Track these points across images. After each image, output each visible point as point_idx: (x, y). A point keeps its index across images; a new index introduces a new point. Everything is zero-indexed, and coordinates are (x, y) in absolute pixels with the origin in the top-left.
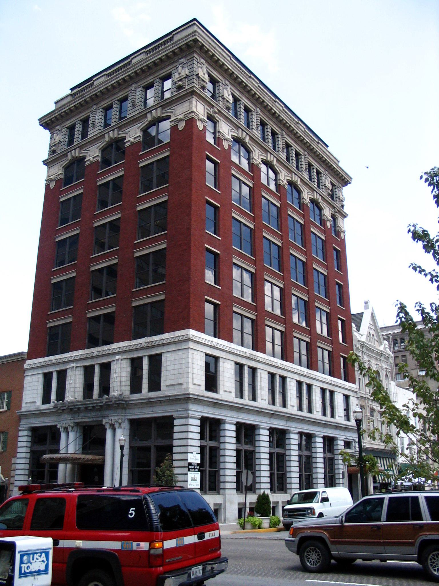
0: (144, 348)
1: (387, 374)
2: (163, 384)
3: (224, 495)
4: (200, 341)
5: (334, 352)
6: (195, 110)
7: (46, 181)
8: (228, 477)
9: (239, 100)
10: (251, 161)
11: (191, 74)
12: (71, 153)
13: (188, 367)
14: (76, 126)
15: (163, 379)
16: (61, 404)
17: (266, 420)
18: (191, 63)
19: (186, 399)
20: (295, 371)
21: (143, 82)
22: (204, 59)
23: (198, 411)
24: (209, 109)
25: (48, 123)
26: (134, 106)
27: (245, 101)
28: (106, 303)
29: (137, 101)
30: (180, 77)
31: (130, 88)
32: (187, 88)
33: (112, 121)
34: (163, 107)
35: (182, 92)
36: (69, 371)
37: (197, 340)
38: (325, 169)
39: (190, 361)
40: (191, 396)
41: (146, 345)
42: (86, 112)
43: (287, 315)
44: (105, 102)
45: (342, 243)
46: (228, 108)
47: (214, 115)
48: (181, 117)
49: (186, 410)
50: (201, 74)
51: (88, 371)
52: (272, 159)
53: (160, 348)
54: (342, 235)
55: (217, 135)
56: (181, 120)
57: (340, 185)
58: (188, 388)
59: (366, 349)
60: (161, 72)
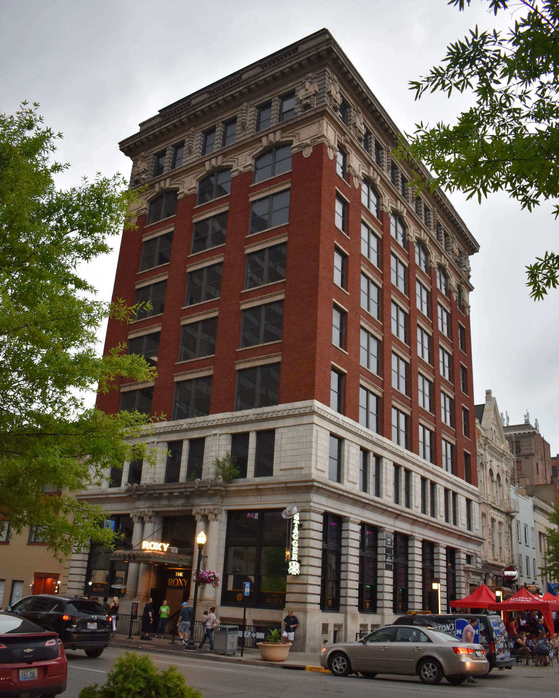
0: (251, 422)
1: (506, 479)
2: (275, 467)
3: (346, 613)
4: (325, 415)
6: (325, 134)
9: (371, 134)
10: (381, 208)
11: (321, 91)
12: (160, 184)
13: (311, 447)
14: (167, 153)
15: (275, 461)
16: (136, 487)
17: (390, 521)
18: (322, 78)
19: (307, 487)
20: (420, 463)
21: (256, 101)
22: (336, 76)
23: (321, 503)
24: (340, 136)
26: (244, 128)
27: (376, 135)
28: (200, 365)
29: (248, 123)
30: (307, 94)
31: (240, 108)
32: (315, 107)
33: (215, 146)
34: (283, 130)
35: (310, 113)
37: (322, 414)
38: (453, 232)
39: (314, 441)
40: (316, 484)
41: (253, 418)
43: (413, 397)
45: (467, 320)
46: (360, 139)
47: (346, 144)
48: (308, 141)
49: (307, 502)
50: (333, 93)
51: (175, 447)
52: (402, 210)
54: (467, 310)
55: (347, 169)
56: (307, 145)
57: (467, 253)
58: (311, 474)
59: (489, 447)
60: (281, 89)
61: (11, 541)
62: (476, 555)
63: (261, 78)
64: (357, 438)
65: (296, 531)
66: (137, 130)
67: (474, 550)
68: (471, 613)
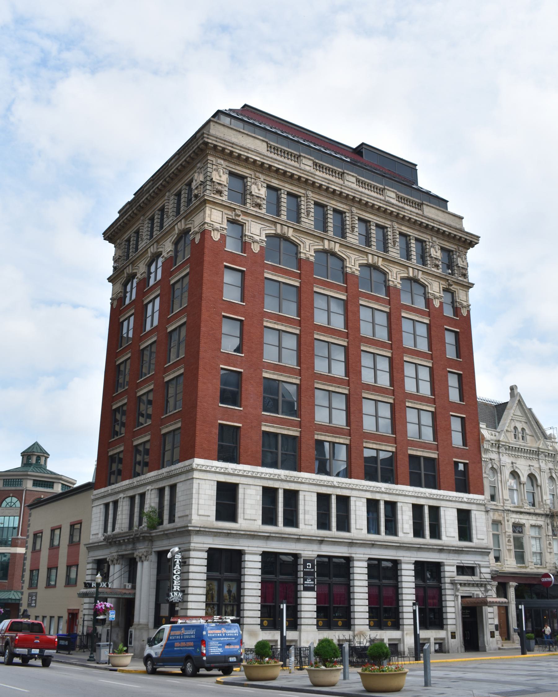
3: (403, 631)
5: (398, 453)
7: (111, 299)
8: (248, 604)
25: (110, 235)
36: (178, 485)
42: (150, 213)
44: (150, 213)
53: (176, 478)
60: (186, 178)
61: (57, 585)
62: (480, 566)
63: (171, 172)
64: (257, 480)
65: (177, 566)
66: (118, 215)
67: (474, 561)
68: (397, 625)
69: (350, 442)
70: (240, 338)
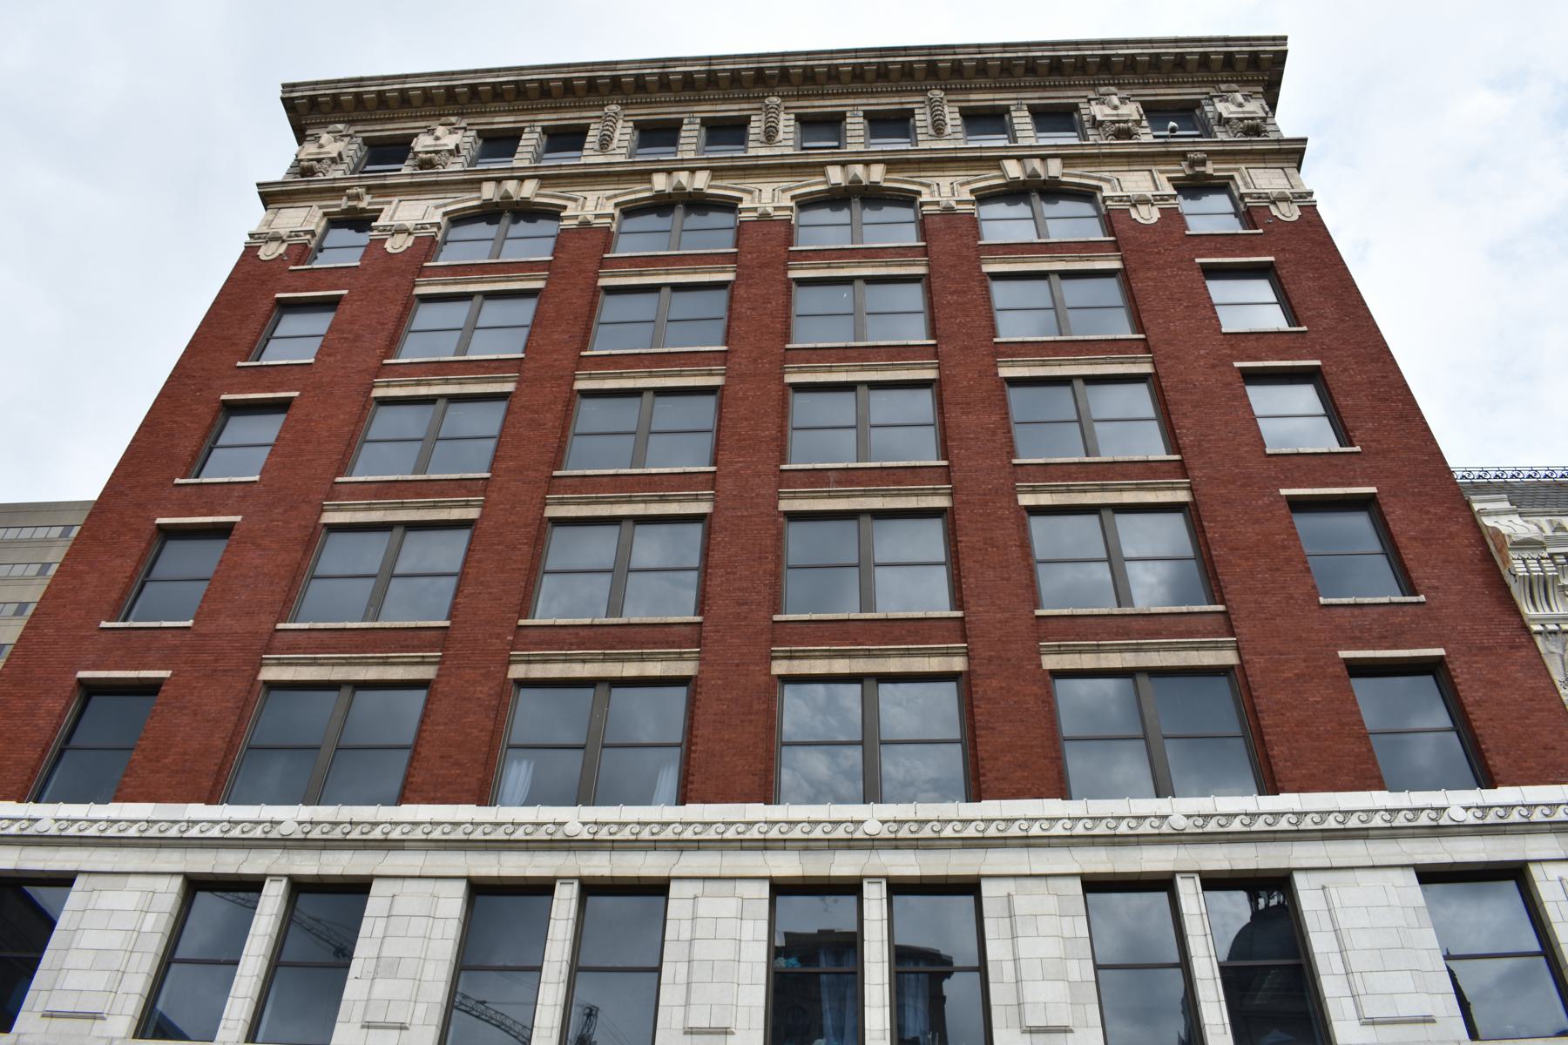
69: (1240, 657)
70: (1328, 415)
